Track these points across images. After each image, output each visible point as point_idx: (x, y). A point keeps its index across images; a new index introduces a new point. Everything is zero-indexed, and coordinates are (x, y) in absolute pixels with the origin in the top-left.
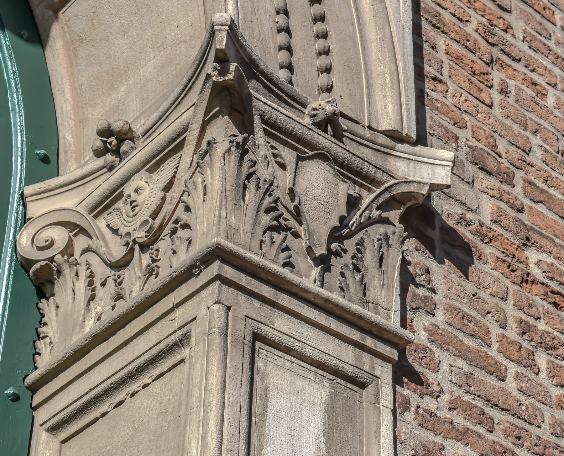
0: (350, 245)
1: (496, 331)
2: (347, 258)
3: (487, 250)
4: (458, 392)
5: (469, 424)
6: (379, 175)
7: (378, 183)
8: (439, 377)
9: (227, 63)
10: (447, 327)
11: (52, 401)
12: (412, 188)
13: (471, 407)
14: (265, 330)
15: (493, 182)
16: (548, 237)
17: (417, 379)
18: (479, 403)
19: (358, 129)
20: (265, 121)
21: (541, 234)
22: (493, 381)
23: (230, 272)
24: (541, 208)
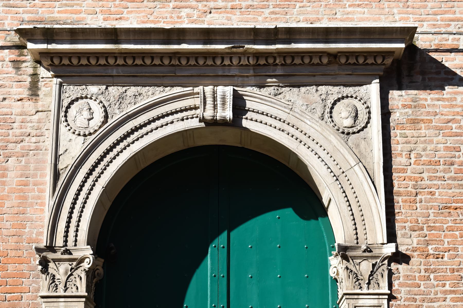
0: (375, 275)
1: (417, 275)
2: (374, 280)
3: (415, 254)
4: (406, 296)
5: (409, 303)
6: (380, 255)
7: (380, 257)
8: (401, 295)
9: (397, 86)
10: (404, 281)
11: (379, 222)
12: (388, 255)
13: (410, 298)
14: (357, 305)
15: (418, 232)
16: (434, 240)
17: (395, 298)
18: (413, 296)
19: (374, 245)
20: (351, 257)
21: (432, 240)
22: (417, 289)
23: (348, 297)
24: (433, 232)
